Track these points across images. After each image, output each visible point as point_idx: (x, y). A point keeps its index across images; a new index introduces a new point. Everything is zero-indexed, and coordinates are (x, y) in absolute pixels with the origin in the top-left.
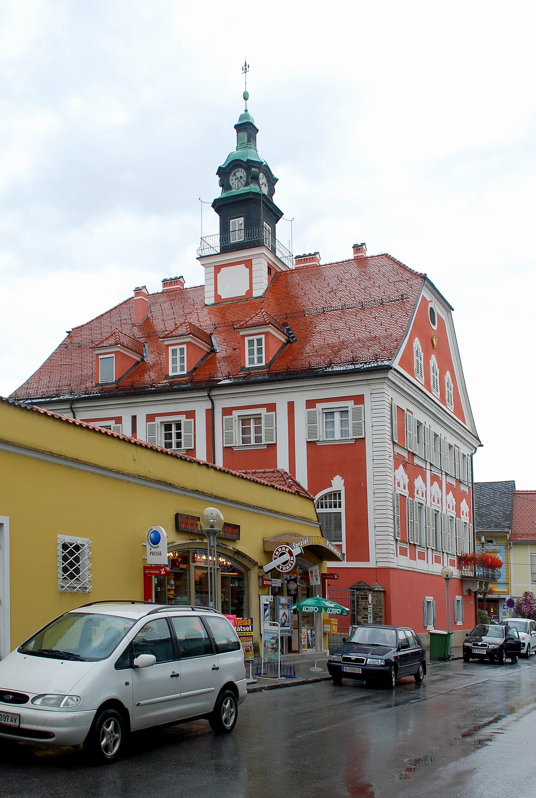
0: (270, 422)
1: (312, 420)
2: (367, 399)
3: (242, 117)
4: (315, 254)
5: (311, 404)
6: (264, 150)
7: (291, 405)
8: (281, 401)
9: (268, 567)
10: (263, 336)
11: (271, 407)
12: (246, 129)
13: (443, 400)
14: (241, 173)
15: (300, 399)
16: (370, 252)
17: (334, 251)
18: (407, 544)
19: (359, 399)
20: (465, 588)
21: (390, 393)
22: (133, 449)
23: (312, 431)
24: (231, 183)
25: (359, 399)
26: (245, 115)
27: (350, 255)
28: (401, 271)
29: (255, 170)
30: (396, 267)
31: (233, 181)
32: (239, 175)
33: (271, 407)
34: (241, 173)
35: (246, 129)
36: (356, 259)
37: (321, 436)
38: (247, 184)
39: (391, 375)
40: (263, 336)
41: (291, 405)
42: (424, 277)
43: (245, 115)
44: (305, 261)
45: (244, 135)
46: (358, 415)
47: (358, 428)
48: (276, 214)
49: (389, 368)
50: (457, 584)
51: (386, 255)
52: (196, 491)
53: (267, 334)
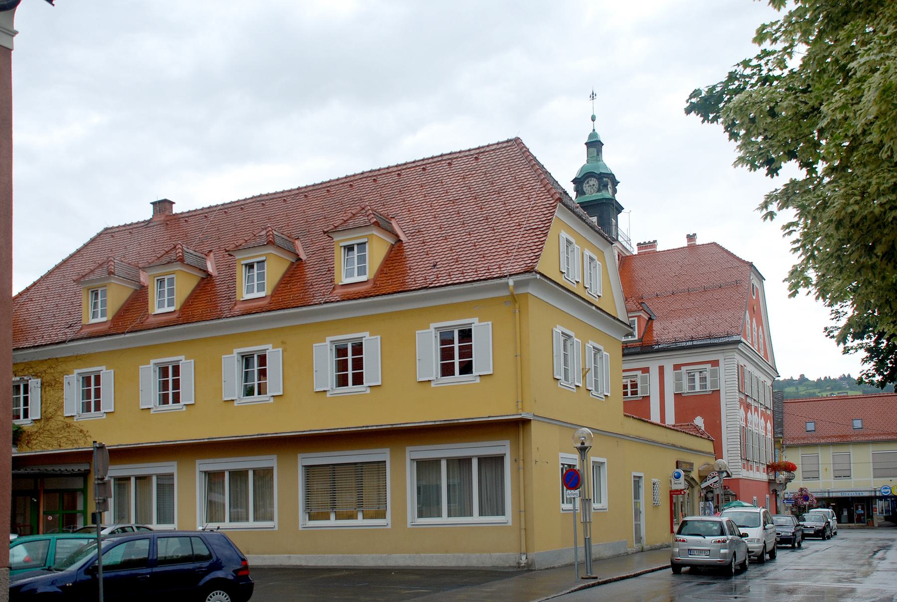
0: (644, 380)
1: (678, 379)
2: (721, 363)
3: (591, 136)
4: (655, 241)
5: (677, 367)
6: (611, 160)
7: (661, 369)
8: (653, 365)
9: (704, 485)
10: (636, 319)
11: (646, 370)
12: (594, 145)
13: (759, 351)
14: (593, 182)
15: (669, 364)
16: (699, 241)
17: (670, 240)
18: (746, 461)
19: (715, 363)
20: (772, 489)
21: (737, 357)
22: (663, 429)
23: (678, 385)
24: (585, 189)
25: (715, 363)
26: (593, 134)
27: (684, 243)
28: (730, 258)
29: (607, 180)
30: (725, 255)
31: (586, 187)
32: (591, 183)
33: (646, 370)
34: (593, 182)
35: (594, 145)
36: (689, 247)
37: (685, 389)
38: (599, 190)
39: (740, 346)
40: (636, 319)
41: (661, 369)
42: (751, 265)
43: (593, 134)
44: (646, 247)
45: (594, 150)
46: (714, 374)
47: (715, 383)
48: (619, 209)
49: (740, 342)
50: (766, 485)
51: (715, 244)
52: (681, 447)
53: (639, 317)
